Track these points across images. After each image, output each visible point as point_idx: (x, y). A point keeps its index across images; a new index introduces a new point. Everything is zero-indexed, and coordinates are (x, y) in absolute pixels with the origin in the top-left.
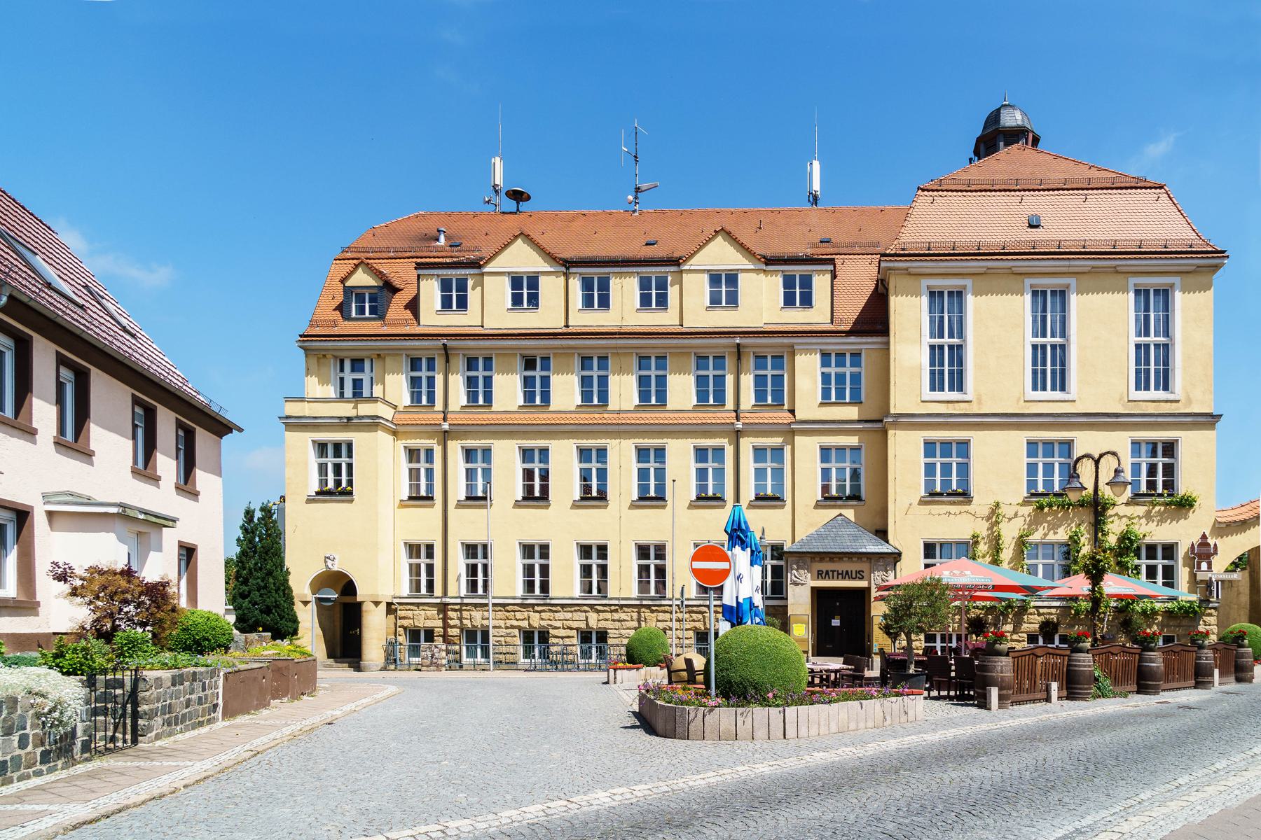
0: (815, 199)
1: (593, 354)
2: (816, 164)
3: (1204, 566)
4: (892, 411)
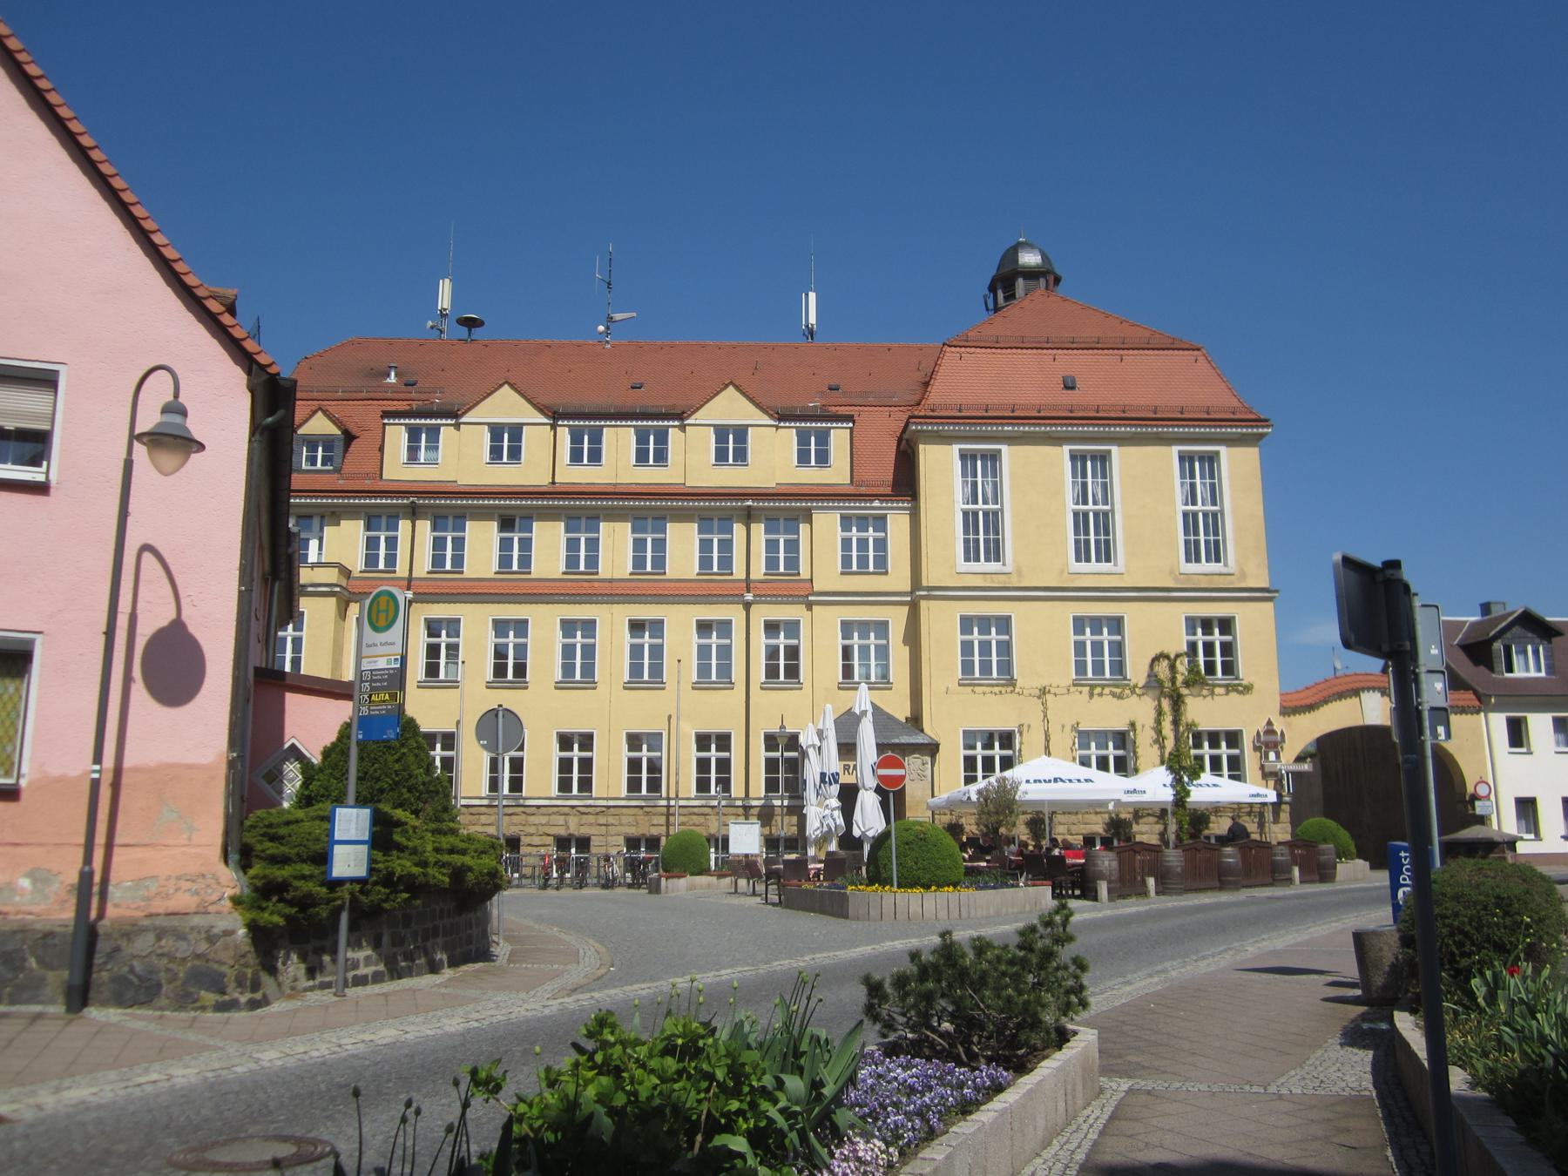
0: (811, 332)
1: (582, 509)
2: (812, 296)
3: (1272, 756)
4: (924, 583)
